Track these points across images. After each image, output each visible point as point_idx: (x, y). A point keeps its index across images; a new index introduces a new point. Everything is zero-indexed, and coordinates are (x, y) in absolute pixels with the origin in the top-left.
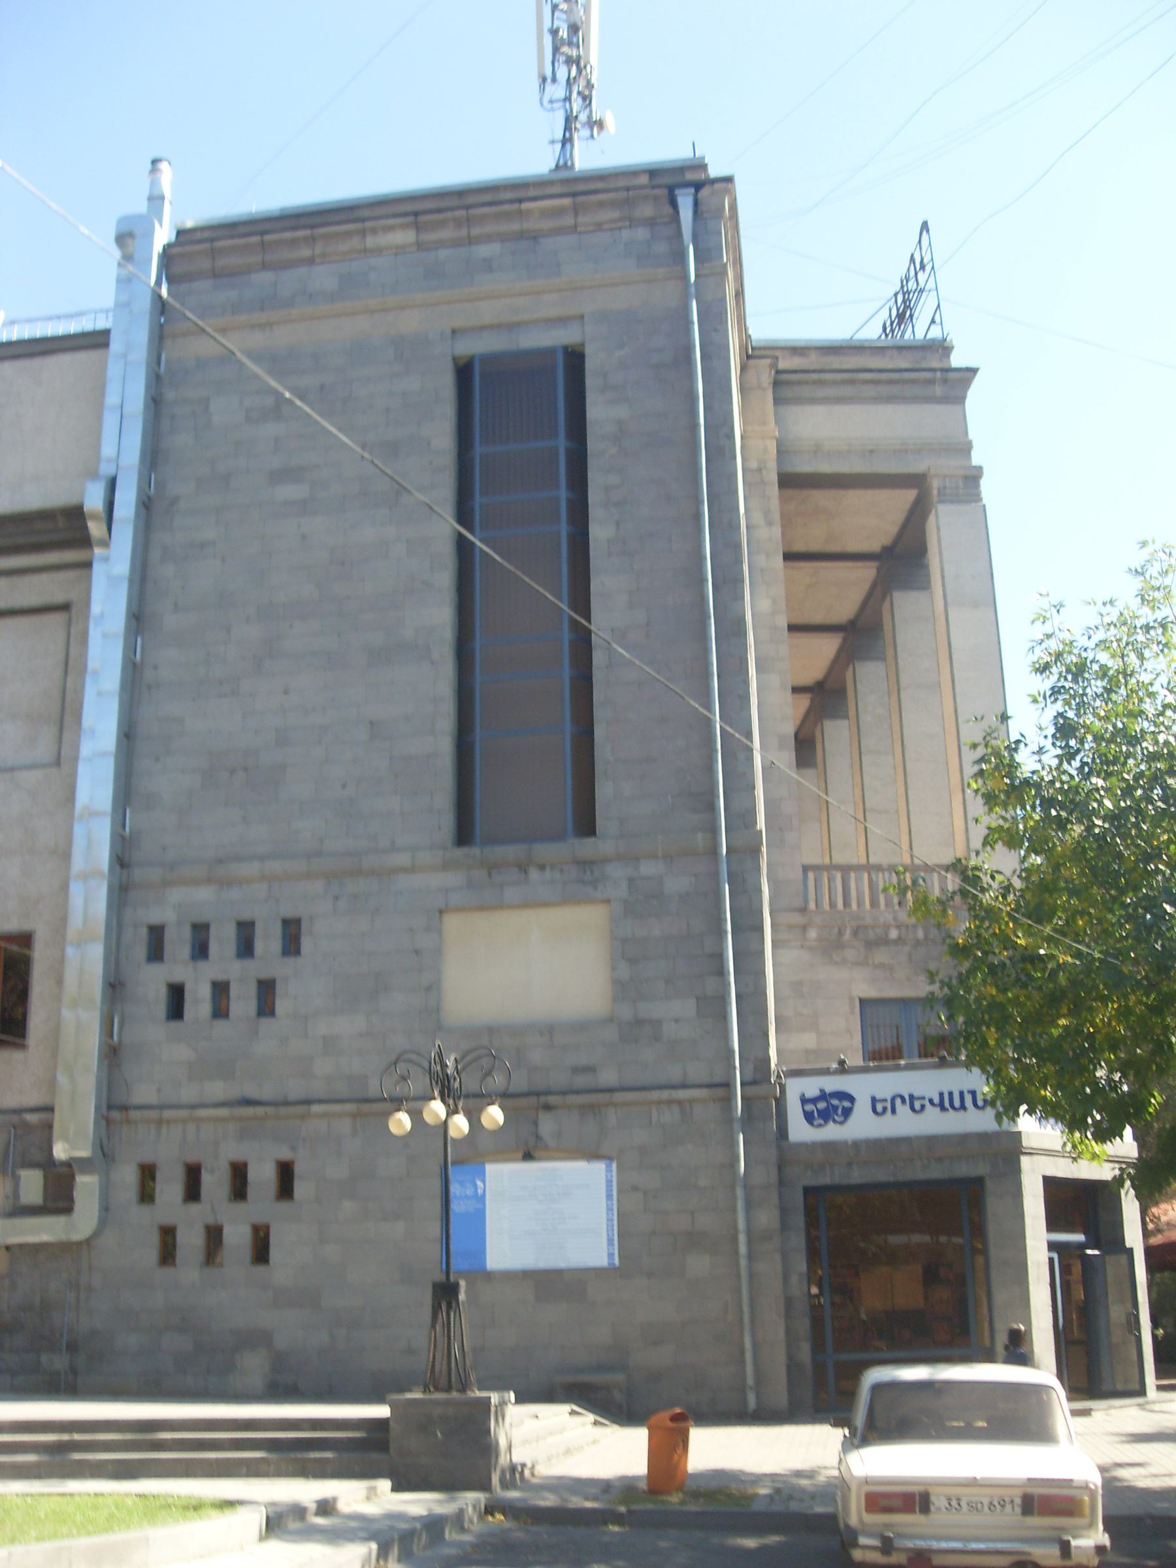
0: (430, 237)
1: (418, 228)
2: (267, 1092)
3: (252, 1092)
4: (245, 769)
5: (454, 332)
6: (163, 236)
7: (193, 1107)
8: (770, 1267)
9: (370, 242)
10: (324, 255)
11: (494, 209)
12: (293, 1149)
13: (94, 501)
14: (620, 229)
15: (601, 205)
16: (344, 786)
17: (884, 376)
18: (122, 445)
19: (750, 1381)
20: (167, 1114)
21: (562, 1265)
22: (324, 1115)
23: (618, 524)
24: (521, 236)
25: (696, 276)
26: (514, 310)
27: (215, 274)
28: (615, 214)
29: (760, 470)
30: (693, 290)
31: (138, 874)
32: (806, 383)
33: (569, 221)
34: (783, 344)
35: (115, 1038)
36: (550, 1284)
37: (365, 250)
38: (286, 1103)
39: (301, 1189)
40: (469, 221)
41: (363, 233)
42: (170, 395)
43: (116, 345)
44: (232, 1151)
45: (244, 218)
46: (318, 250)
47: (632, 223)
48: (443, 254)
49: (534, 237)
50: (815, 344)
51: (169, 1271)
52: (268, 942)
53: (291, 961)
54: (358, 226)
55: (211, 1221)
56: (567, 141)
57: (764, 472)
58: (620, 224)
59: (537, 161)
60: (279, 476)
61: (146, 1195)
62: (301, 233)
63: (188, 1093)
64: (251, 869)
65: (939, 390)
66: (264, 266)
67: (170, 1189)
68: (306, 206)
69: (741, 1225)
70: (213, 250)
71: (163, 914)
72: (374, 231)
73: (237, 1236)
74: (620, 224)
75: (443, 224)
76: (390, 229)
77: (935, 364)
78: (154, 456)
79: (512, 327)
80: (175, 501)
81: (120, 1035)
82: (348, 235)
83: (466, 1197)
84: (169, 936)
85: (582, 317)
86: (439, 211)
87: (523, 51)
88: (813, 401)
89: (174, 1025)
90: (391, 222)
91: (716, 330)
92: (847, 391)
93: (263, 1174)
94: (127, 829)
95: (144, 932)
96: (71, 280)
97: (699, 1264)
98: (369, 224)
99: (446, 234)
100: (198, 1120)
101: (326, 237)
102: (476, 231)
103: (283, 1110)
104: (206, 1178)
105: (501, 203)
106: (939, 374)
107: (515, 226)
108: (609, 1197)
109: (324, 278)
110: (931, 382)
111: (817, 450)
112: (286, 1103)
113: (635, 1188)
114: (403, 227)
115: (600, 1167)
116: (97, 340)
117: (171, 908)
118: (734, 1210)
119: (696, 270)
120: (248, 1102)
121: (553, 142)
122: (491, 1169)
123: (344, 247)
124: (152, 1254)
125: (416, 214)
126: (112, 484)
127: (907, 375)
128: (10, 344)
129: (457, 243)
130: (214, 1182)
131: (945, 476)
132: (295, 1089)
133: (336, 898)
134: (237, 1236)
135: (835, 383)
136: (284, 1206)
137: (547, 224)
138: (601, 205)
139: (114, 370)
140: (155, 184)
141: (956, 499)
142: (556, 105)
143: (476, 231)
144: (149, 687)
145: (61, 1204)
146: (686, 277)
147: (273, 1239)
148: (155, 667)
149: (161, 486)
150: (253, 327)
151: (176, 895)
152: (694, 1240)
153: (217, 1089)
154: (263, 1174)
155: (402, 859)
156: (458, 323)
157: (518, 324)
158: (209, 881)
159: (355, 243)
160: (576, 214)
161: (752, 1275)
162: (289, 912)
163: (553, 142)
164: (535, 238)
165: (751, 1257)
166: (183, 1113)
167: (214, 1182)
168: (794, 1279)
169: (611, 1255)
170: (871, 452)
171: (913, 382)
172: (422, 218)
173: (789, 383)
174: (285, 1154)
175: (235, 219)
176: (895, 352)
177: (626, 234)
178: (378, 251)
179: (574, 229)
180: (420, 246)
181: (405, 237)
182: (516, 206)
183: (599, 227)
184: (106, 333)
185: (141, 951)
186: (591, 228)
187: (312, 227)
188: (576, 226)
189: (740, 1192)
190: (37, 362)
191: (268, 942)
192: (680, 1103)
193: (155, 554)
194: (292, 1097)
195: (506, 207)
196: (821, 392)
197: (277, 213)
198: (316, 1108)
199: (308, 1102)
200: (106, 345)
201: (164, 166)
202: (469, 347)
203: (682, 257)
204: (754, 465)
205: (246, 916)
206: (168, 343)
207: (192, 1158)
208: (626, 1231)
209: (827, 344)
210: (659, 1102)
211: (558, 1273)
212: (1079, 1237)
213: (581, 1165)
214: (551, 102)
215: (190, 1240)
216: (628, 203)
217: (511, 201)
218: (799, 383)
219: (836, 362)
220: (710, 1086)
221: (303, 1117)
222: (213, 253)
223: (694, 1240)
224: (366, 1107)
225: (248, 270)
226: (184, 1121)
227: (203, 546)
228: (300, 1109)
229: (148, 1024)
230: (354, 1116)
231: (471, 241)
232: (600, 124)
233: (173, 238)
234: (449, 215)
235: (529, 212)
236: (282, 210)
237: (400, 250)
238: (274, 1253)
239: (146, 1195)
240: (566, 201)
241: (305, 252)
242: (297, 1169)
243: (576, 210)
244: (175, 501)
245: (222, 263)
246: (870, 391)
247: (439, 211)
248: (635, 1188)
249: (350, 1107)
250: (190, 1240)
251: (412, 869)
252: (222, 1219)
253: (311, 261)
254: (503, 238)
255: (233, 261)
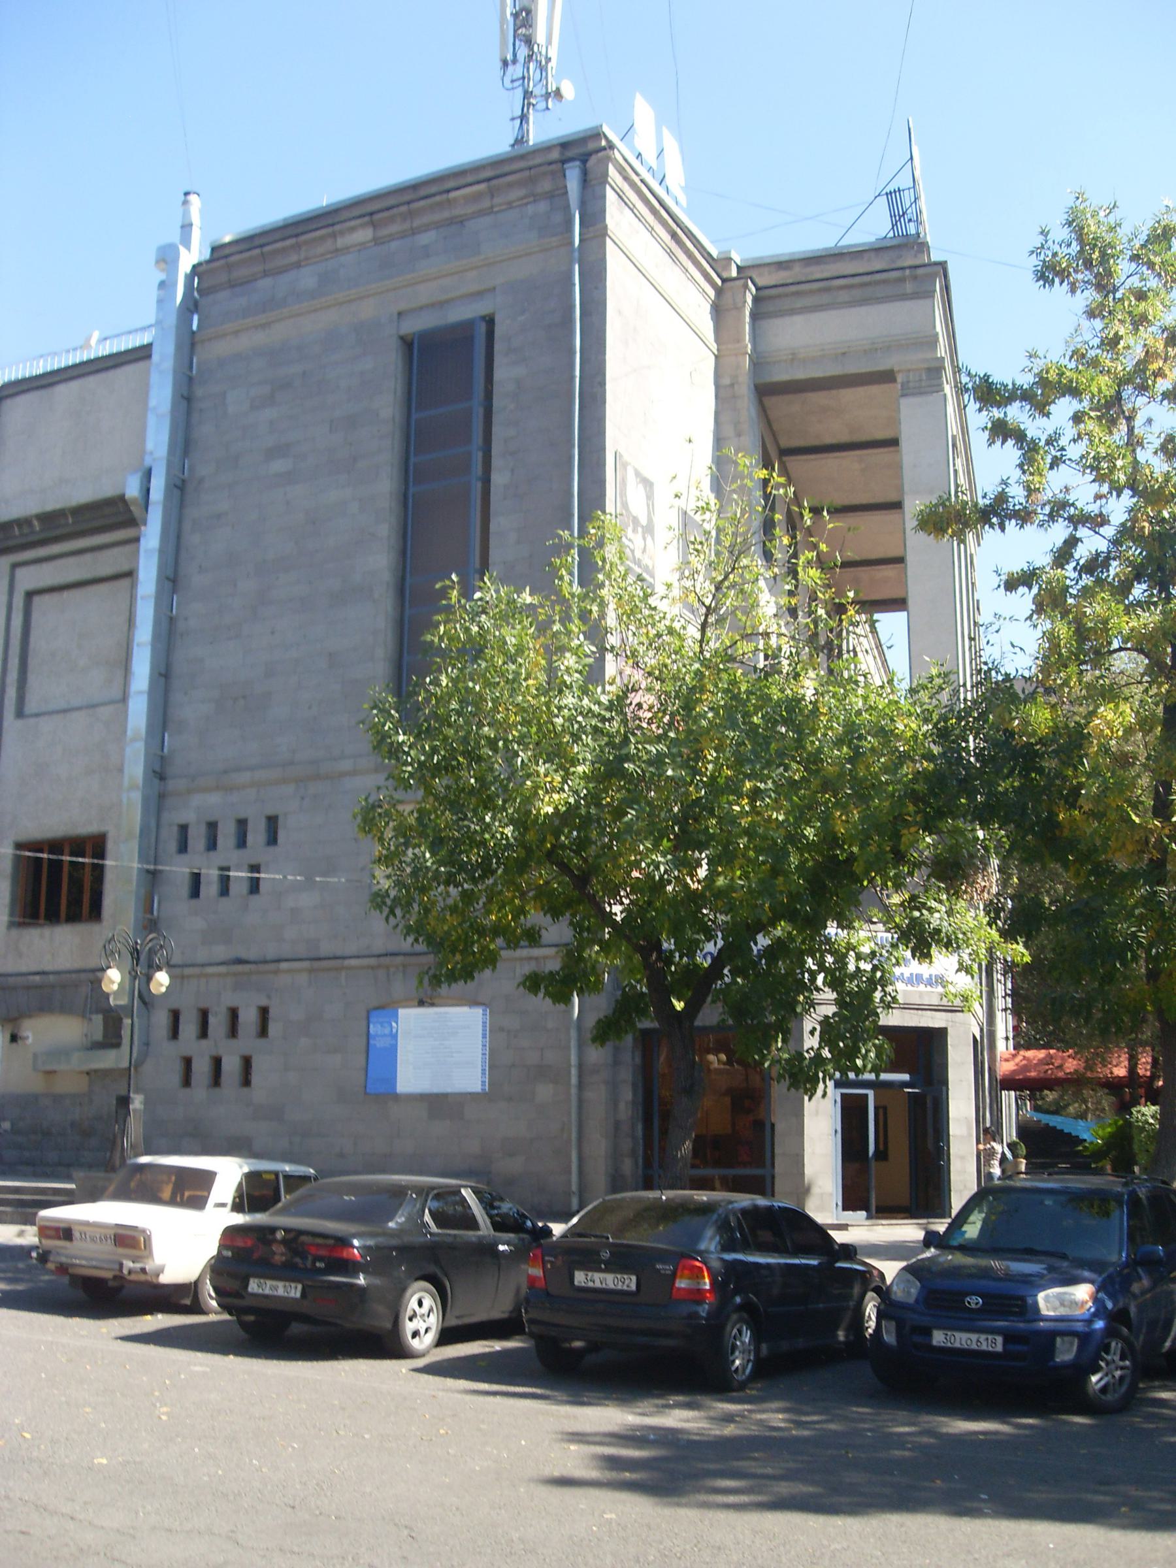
0: (384, 232)
1: (374, 225)
2: (252, 954)
3: (244, 955)
4: (244, 697)
5: (400, 314)
6: (188, 259)
7: (203, 965)
8: (597, 1095)
9: (340, 242)
10: (306, 259)
11: (429, 201)
12: (269, 997)
13: (132, 490)
14: (527, 204)
15: (510, 185)
16: (310, 708)
17: (857, 280)
18: (157, 441)
19: (574, 1187)
20: (187, 971)
21: (449, 1090)
22: (289, 971)
23: (512, 471)
24: (451, 222)
25: (581, 241)
26: (440, 289)
27: (232, 285)
28: (522, 192)
29: (732, 385)
30: (576, 254)
31: (171, 785)
32: (786, 295)
33: (486, 203)
34: (768, 261)
35: (155, 913)
36: (438, 1104)
37: (337, 250)
38: (265, 962)
39: (273, 1028)
40: (411, 214)
41: (334, 236)
42: (199, 392)
43: (156, 357)
44: (230, 999)
45: (258, 231)
46: (303, 255)
47: (536, 198)
48: (394, 245)
49: (460, 221)
50: (797, 257)
51: (187, 1090)
52: (257, 835)
53: (271, 849)
54: (330, 230)
55: (214, 1053)
56: (523, 118)
57: (736, 386)
58: (525, 201)
59: (494, 141)
60: (278, 451)
61: (175, 1033)
62: (288, 242)
63: (202, 955)
64: (245, 777)
65: (909, 287)
66: (266, 274)
67: (189, 1028)
68: (300, 215)
69: (574, 1059)
70: (262, 254)
71: (188, 815)
72: (342, 233)
73: (231, 1065)
74: (525, 201)
75: (392, 220)
76: (353, 229)
77: (909, 262)
78: (184, 443)
79: (441, 305)
80: (201, 480)
81: (159, 911)
82: (322, 239)
83: (385, 1035)
84: (192, 832)
85: (494, 288)
86: (388, 209)
87: (489, 35)
88: (792, 312)
89: (194, 902)
90: (353, 223)
91: (596, 288)
92: (825, 298)
93: (249, 1018)
94: (166, 750)
95: (175, 829)
96: (121, 305)
97: (545, 1092)
98: (337, 228)
99: (394, 228)
100: (207, 975)
101: (306, 243)
102: (417, 222)
103: (262, 967)
104: (212, 1020)
105: (434, 195)
106: (907, 272)
107: (446, 214)
108: (484, 1036)
109: (307, 279)
110: (902, 280)
111: (794, 358)
112: (265, 962)
113: (501, 1029)
114: (363, 226)
115: (478, 1012)
116: (143, 353)
117: (191, 811)
118: (568, 1048)
119: (580, 235)
120: (240, 961)
121: (513, 119)
122: (402, 1012)
123: (320, 250)
124: (176, 1078)
125: (371, 214)
126: (148, 474)
127: (878, 277)
128: (127, 352)
129: (403, 235)
130: (218, 1023)
131: (909, 371)
132: (271, 952)
133: (303, 798)
134: (231, 1065)
135: (811, 292)
136: (262, 1042)
137: (470, 209)
138: (510, 185)
139: (154, 378)
140: (186, 214)
141: (920, 392)
142: (516, 84)
143: (417, 222)
144: (182, 635)
145: (114, 1041)
146: (572, 243)
147: (254, 1065)
148: (186, 619)
149: (191, 469)
150: (256, 327)
151: (197, 800)
152: (542, 1072)
153: (221, 952)
154: (249, 1018)
155: (346, 765)
156: (403, 306)
157: (447, 302)
158: (217, 788)
159: (329, 245)
160: (492, 196)
161: (581, 1101)
162: (271, 811)
163: (513, 119)
164: (461, 222)
165: (581, 1086)
166: (197, 970)
167: (218, 1023)
168: (622, 1106)
169: (483, 1083)
170: (844, 354)
171: (885, 281)
172: (376, 217)
173: (770, 298)
174: (264, 1002)
175: (251, 233)
176: (873, 254)
177: (530, 209)
178: (346, 249)
179: (490, 211)
180: (377, 241)
181: (364, 235)
182: (445, 196)
183: (510, 205)
184: (149, 346)
185: (173, 846)
186: (504, 207)
187: (297, 236)
188: (492, 207)
189: (573, 1034)
190: (111, 374)
191: (257, 835)
192: (537, 959)
193: (187, 526)
194: (269, 957)
195: (438, 198)
196: (799, 303)
197: (281, 224)
198: (284, 966)
199: (278, 961)
200: (149, 356)
201: (193, 198)
202: (412, 326)
203: (569, 223)
204: (726, 381)
205: (242, 816)
206: (198, 348)
207: (203, 1005)
208: (494, 1065)
209: (803, 256)
210: (521, 959)
211: (445, 1095)
212: (906, 1077)
213: (465, 1009)
214: (513, 81)
215: (201, 1068)
216: (532, 180)
217: (441, 193)
218: (779, 296)
219: (818, 272)
220: (556, 946)
221: (276, 972)
222: (229, 267)
223: (542, 1072)
224: (316, 964)
225: (253, 279)
226: (199, 976)
227: (219, 516)
228: (272, 966)
229: (174, 904)
230: (311, 971)
231: (414, 232)
232: (558, 93)
233: (207, 255)
234: (395, 211)
235: (455, 199)
236: (285, 219)
237: (362, 246)
238: (255, 1078)
239: (175, 1033)
240: (482, 186)
241: (294, 258)
242: (272, 1013)
243: (492, 193)
244: (201, 480)
245: (243, 270)
246: (844, 296)
247: (388, 209)
248: (501, 1029)
249: (306, 964)
250: (201, 1068)
251: (354, 773)
252: (221, 1052)
253: (298, 265)
254: (437, 226)
255: (243, 272)
